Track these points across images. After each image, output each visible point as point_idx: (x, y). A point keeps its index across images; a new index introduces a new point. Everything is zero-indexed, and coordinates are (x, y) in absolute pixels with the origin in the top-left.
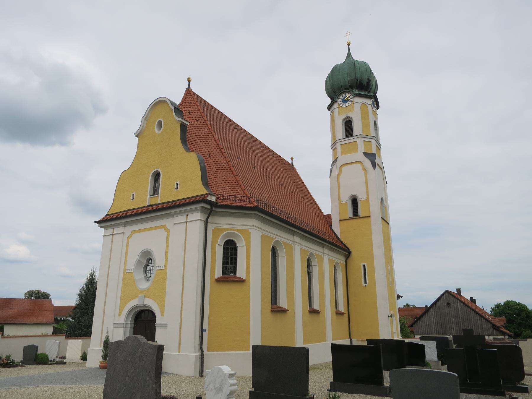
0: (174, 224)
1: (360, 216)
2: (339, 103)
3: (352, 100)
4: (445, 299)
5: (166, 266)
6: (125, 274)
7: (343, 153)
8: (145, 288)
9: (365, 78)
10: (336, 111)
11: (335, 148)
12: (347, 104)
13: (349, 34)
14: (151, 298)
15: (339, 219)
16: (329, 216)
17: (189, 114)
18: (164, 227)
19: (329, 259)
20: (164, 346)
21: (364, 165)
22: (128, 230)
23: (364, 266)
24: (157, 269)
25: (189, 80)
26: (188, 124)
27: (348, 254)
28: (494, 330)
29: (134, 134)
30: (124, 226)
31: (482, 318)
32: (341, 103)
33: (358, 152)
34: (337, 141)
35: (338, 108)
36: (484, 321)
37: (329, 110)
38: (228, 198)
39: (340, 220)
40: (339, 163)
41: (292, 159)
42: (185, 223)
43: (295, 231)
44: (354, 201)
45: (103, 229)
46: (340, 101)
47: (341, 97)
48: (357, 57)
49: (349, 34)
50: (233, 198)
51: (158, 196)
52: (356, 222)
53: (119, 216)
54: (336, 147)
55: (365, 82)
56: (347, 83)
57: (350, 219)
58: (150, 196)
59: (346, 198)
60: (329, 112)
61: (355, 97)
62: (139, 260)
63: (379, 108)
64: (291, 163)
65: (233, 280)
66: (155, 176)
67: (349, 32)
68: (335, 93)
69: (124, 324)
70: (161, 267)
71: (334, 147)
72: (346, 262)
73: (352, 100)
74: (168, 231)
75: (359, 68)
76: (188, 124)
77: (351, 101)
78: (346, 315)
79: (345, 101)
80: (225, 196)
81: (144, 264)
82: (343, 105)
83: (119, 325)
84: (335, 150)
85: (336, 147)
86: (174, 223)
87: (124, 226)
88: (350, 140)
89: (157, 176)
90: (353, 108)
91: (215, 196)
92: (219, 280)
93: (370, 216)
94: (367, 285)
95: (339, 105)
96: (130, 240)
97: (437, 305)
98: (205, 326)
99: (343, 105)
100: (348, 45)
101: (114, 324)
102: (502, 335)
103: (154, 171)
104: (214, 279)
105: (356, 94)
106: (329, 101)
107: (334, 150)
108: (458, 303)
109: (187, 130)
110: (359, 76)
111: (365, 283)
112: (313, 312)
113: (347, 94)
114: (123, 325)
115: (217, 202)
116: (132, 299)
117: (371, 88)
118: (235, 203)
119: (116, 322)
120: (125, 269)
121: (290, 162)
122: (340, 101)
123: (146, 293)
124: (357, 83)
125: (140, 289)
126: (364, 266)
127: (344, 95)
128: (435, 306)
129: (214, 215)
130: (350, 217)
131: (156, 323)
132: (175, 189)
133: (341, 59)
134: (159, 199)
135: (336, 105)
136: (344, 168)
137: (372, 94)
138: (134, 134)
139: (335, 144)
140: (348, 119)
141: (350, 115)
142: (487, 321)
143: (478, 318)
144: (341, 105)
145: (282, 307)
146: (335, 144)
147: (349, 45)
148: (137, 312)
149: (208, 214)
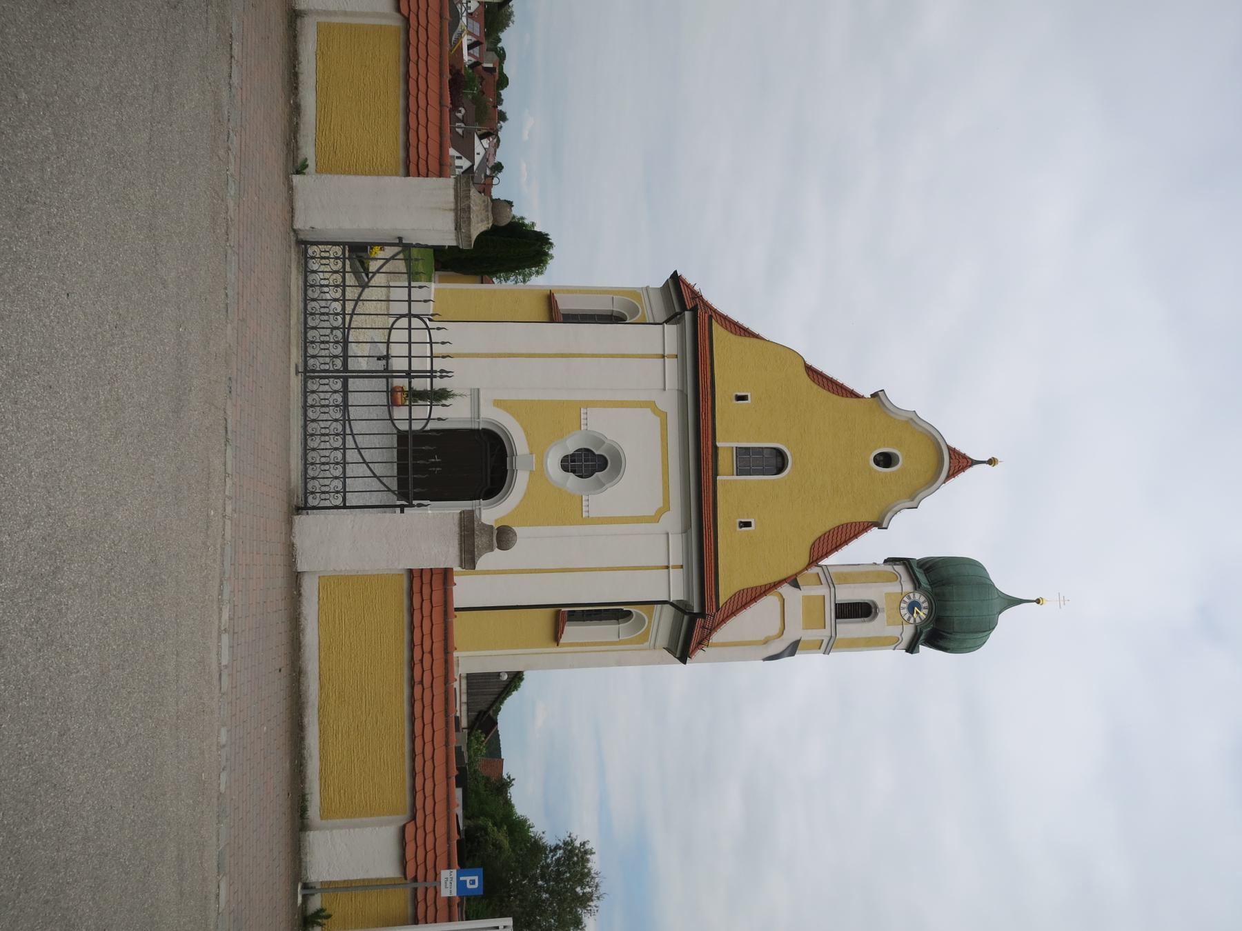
0: (668, 534)
2: (911, 595)
3: (912, 621)
7: (807, 599)
8: (547, 468)
12: (904, 612)
13: (1062, 603)
14: (528, 488)
21: (776, 640)
25: (992, 462)
28: (476, 713)
31: (496, 696)
32: (909, 598)
34: (832, 589)
36: (491, 698)
42: (666, 564)
47: (922, 599)
48: (1006, 619)
49: (1062, 603)
56: (948, 613)
61: (916, 627)
62: (604, 442)
73: (912, 621)
74: (655, 519)
79: (912, 606)
81: (597, 451)
82: (905, 602)
83: (476, 408)
84: (817, 576)
89: (778, 461)
90: (894, 624)
95: (908, 595)
99: (905, 602)
101: (478, 389)
102: (468, 722)
105: (921, 632)
110: (958, 636)
113: (926, 611)
114: (476, 416)
116: (527, 435)
119: (481, 392)
123: (539, 475)
124: (944, 632)
125: (547, 457)
127: (926, 605)
129: (675, 617)
131: (481, 500)
139: (830, 581)
140: (873, 610)
141: (882, 617)
142: (491, 703)
143: (496, 690)
144: (905, 599)
146: (830, 581)
147: (1038, 601)
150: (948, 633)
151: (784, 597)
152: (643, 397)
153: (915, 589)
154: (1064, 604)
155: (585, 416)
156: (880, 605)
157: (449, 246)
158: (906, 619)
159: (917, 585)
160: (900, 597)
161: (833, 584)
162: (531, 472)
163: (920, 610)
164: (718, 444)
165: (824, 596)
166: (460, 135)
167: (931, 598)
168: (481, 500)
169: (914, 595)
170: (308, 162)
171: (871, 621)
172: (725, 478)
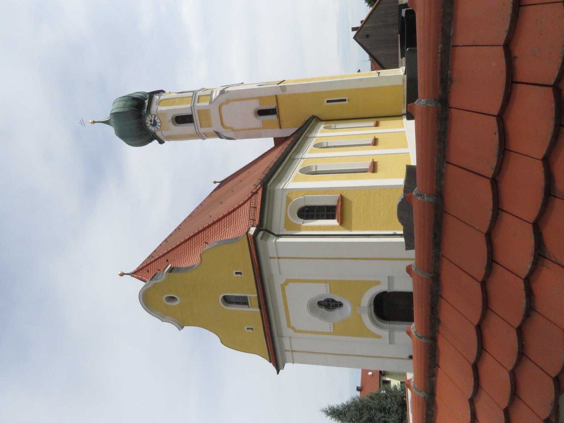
0: (280, 273)
1: (276, 107)
2: (156, 130)
3: (153, 116)
4: (362, 40)
5: (325, 282)
6: (335, 333)
7: (210, 126)
9: (129, 103)
10: (165, 133)
11: (204, 135)
12: (158, 121)
13: (82, 122)
15: (279, 129)
16: (276, 139)
17: (160, 270)
18: (283, 286)
19: (322, 133)
20: (406, 165)
22: (286, 331)
23: (328, 101)
24: (329, 292)
25: (122, 274)
26: (170, 265)
27: (315, 119)
29: (180, 330)
30: (282, 337)
31: (381, 2)
33: (209, 109)
35: (162, 132)
37: (164, 142)
38: (252, 213)
39: (280, 128)
40: (221, 130)
41: (215, 182)
43: (290, 157)
44: (261, 113)
45: (286, 364)
46: (155, 129)
47: (151, 128)
48: (106, 116)
49: (82, 122)
50: (252, 215)
51: (249, 296)
52: (282, 111)
53: (272, 347)
54: (204, 133)
55: (135, 103)
57: (279, 117)
58: (249, 307)
59: (258, 121)
60: (166, 142)
61: (150, 113)
63: (164, 90)
64: (219, 183)
65: (341, 207)
66: (227, 303)
67: (80, 123)
68: (147, 134)
69: (390, 331)
70: (331, 326)
71: (204, 136)
72: (323, 121)
73: (153, 116)
74: (288, 281)
75: (119, 108)
76: (170, 265)
77: (155, 117)
78: (378, 119)
79: (155, 124)
80: (250, 218)
82: (159, 126)
85: (204, 133)
86: (279, 273)
87: (282, 337)
88: (196, 118)
89: (227, 300)
91: (250, 228)
92: (342, 222)
93: (276, 96)
94: (347, 98)
96: (298, 328)
97: (368, 47)
98: (391, 233)
99: (159, 126)
100: (94, 123)
103: (222, 305)
104: (340, 226)
106: (155, 142)
107: (206, 136)
108: (366, 27)
109: (178, 267)
111: (345, 100)
112: (375, 142)
115: (256, 226)
117: (142, 97)
118: (258, 207)
119: (388, 342)
120: (330, 333)
121: (218, 184)
122: (155, 129)
123: (356, 304)
124: (136, 110)
126: (328, 101)
127: (148, 125)
128: (369, 50)
129: (271, 227)
130: (277, 118)
131: (388, 292)
132: (242, 276)
133: (111, 130)
134: (252, 295)
135: (159, 134)
136: (226, 124)
137: (148, 96)
138: (180, 330)
141: (169, 118)
144: (159, 128)
145: (370, 166)
148: (378, 318)
149: (270, 234)
150: (133, 110)
152: (300, 335)
153: (155, 133)
154: (81, 121)
155: (331, 328)
157: (413, 310)
158: (156, 117)
159: (155, 136)
161: (197, 134)
162: (359, 305)
164: (258, 310)
168: (388, 292)
169: (155, 130)
170: (260, 240)
172: (253, 295)
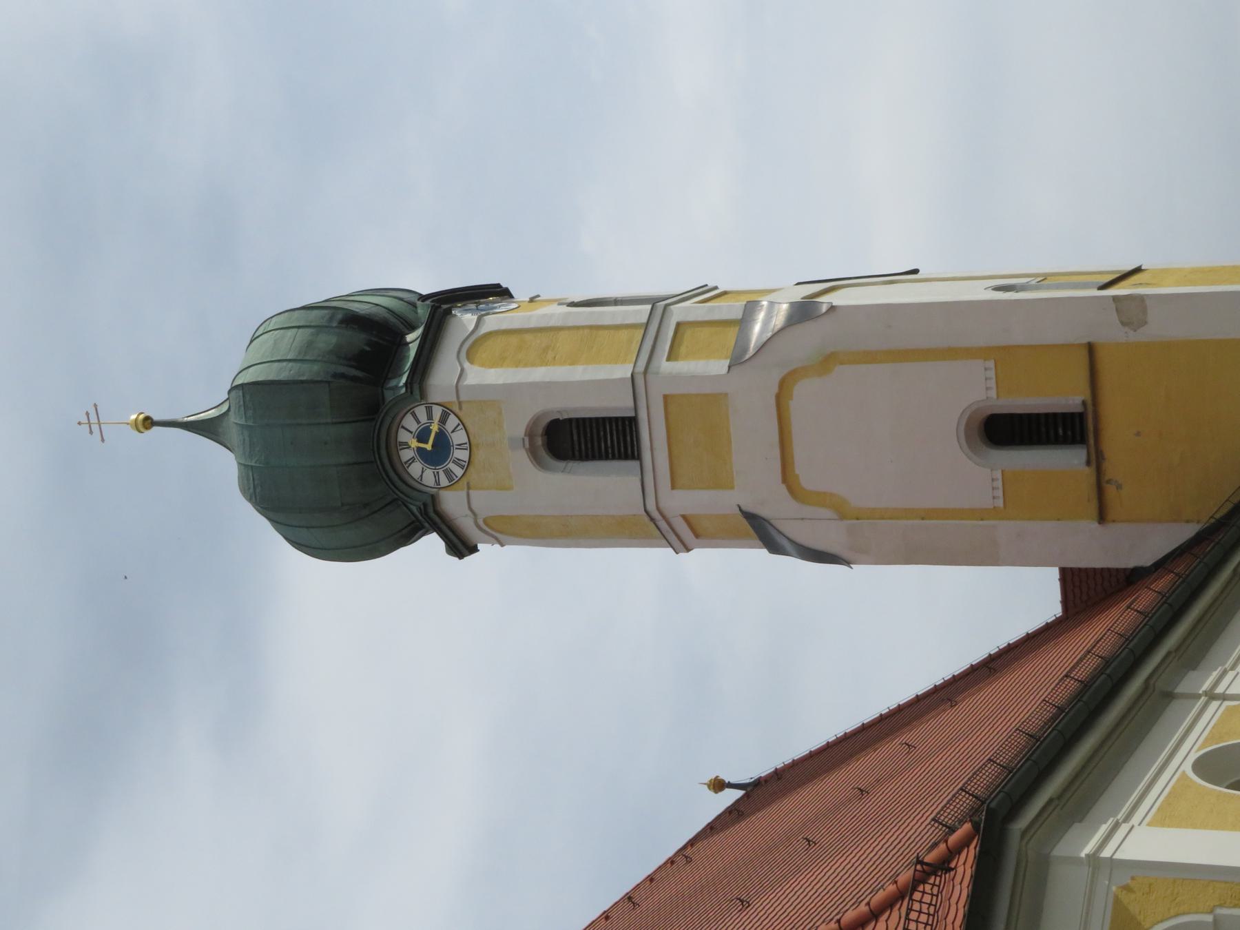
2: (444, 481)
3: (437, 412)
7: (720, 480)
12: (458, 437)
13: (93, 419)
32: (449, 474)
49: (93, 419)
56: (347, 430)
73: (437, 412)
79: (439, 452)
82: (458, 462)
99: (458, 462)
122: (436, 476)
124: (354, 379)
139: (663, 524)
144: (458, 472)
146: (663, 524)
147: (149, 423)
150: (343, 376)
151: (783, 488)
153: (434, 499)
154: (87, 414)
156: (522, 458)
158: (452, 417)
160: (473, 474)
163: (419, 448)
165: (673, 487)
166: (746, 796)
167: (403, 487)
169: (437, 482)
171: (544, 414)
